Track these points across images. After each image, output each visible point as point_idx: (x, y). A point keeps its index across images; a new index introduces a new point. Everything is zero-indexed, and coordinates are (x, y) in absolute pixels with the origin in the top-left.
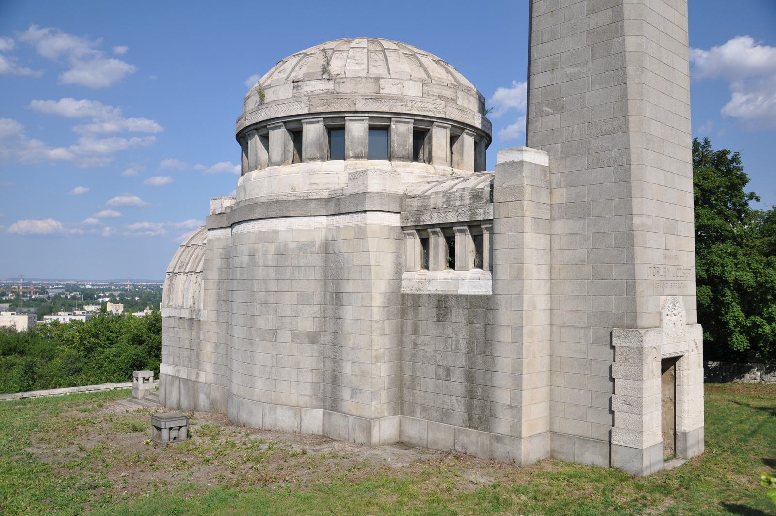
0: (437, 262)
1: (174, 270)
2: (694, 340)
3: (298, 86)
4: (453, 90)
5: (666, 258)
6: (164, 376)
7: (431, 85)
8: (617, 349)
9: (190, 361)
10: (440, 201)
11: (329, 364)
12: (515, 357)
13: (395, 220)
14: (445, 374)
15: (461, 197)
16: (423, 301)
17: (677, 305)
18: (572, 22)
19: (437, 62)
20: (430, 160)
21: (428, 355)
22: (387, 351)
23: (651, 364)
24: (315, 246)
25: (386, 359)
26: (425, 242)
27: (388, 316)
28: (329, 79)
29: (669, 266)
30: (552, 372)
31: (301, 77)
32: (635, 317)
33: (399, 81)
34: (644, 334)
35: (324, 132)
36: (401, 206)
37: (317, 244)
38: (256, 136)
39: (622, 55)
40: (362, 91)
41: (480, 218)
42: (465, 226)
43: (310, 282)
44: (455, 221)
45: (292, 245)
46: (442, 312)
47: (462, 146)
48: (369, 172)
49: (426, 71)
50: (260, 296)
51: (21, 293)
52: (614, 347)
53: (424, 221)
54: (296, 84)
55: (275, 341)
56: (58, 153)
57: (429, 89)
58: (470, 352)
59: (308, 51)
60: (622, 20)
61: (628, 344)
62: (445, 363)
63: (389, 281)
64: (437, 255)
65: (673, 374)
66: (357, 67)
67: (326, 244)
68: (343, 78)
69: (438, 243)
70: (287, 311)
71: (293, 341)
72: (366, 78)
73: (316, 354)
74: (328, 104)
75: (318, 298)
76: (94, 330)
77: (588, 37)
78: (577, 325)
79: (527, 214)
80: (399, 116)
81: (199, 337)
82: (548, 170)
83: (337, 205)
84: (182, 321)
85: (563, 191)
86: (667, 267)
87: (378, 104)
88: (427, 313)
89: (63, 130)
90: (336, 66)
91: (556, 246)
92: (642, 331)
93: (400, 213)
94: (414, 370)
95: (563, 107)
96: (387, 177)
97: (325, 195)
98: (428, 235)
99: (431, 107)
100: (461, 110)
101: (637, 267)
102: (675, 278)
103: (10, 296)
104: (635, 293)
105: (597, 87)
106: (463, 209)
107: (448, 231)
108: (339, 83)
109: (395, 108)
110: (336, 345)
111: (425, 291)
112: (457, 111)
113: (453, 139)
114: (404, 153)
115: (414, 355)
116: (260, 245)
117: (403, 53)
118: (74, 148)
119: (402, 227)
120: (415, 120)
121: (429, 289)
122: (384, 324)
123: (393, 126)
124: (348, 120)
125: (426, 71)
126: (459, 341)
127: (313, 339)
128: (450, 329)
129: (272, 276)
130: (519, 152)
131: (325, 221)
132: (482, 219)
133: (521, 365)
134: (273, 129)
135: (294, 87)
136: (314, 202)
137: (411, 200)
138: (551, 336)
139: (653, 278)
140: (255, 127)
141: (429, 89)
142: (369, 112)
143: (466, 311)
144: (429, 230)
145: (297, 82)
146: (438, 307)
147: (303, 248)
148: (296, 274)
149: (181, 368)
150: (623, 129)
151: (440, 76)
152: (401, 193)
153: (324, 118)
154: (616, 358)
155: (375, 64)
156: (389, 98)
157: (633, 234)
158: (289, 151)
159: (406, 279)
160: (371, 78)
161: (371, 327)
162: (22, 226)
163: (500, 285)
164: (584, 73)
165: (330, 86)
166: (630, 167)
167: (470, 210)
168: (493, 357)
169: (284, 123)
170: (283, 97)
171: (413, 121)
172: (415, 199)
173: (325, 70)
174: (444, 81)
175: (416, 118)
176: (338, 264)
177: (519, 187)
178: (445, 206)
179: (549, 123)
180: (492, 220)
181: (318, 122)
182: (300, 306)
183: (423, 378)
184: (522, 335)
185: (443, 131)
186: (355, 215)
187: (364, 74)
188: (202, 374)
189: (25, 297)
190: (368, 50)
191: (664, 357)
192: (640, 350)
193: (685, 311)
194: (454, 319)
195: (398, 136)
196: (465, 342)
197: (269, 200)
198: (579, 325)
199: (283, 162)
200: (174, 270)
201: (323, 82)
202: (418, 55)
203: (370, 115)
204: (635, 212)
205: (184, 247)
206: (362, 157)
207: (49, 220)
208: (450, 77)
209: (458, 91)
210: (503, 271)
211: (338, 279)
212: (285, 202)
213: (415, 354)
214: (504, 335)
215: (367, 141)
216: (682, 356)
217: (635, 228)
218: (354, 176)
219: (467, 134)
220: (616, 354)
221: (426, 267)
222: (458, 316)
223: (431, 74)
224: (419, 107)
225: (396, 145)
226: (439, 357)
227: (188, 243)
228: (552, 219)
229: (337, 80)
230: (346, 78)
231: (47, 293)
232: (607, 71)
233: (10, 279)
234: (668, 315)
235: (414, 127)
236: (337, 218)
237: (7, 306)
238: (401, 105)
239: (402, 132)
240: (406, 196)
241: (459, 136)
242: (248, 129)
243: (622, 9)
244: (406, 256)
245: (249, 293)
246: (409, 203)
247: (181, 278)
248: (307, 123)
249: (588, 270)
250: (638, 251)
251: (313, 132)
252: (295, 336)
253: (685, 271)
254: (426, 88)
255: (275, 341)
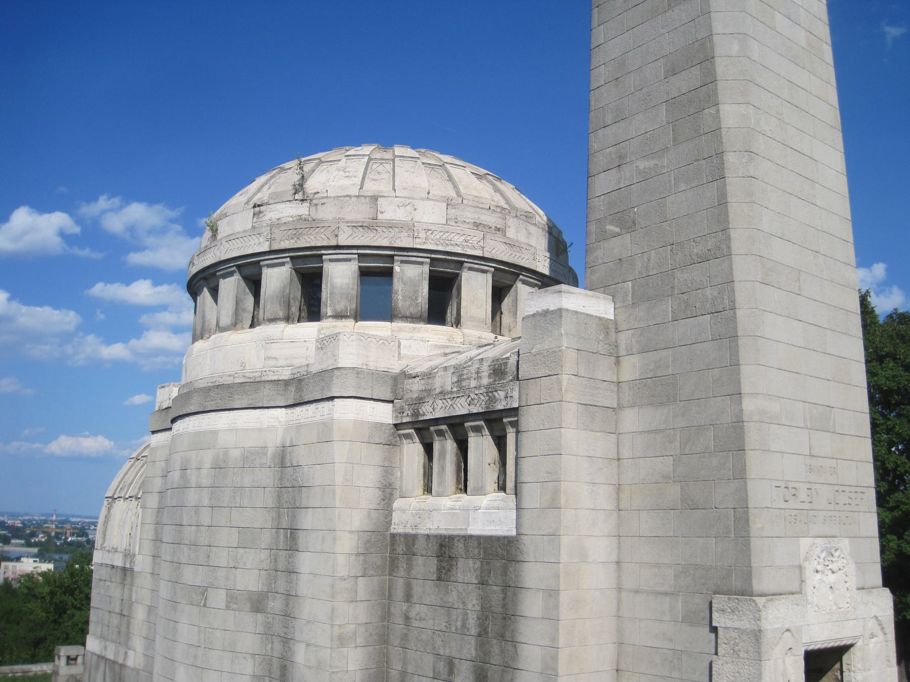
0: (441, 483)
1: (114, 493)
2: (876, 617)
3: (260, 212)
4: (500, 215)
5: (811, 470)
6: (90, 655)
7: (462, 207)
8: (720, 633)
9: (119, 632)
10: (446, 381)
11: (278, 645)
12: (548, 644)
13: (384, 414)
14: (446, 669)
15: (478, 373)
16: (420, 545)
17: (836, 554)
18: (644, 91)
19: (479, 177)
20: (457, 323)
21: (424, 637)
22: (361, 629)
23: (780, 661)
24: (265, 454)
25: (358, 641)
26: (428, 449)
27: (365, 569)
28: (303, 200)
29: (818, 486)
30: (620, 673)
31: (266, 199)
32: (748, 575)
33: (408, 201)
34: (764, 606)
35: (291, 280)
36: (394, 391)
37: (270, 451)
38: (205, 289)
39: (716, 132)
40: (349, 217)
41: (500, 406)
42: (479, 420)
43: (256, 513)
44: (464, 412)
45: (235, 454)
46: (445, 564)
47: (516, 300)
48: (341, 337)
49: (455, 187)
50: (189, 533)
51: (53, 534)
52: (714, 630)
53: (424, 414)
54: (257, 209)
55: (205, 606)
56: (117, 351)
57: (458, 213)
58: (483, 633)
59: (287, 165)
60: (714, 81)
61: (737, 624)
62: (447, 652)
63: (369, 514)
64: (443, 468)
65: (839, 677)
66: (346, 182)
67: (283, 451)
68: (323, 198)
69: (446, 447)
70: (222, 558)
71: (228, 608)
72: (358, 197)
73: (260, 629)
74: (298, 236)
75: (266, 538)
76: (67, 582)
77: (667, 111)
78: (658, 589)
79: (569, 396)
80: (405, 253)
81: (131, 596)
82: (612, 326)
83: (303, 390)
84: (114, 570)
85: (635, 359)
86: (813, 486)
87: (372, 235)
88: (425, 565)
89: (126, 322)
90: (313, 184)
91: (626, 453)
92: (760, 601)
93: (392, 402)
94: (405, 663)
95: (634, 223)
96: (372, 345)
97: (286, 375)
98: (432, 438)
99: (459, 239)
100: (511, 245)
101: (751, 486)
102: (831, 507)
103: (41, 538)
104: (748, 532)
105: (683, 187)
106: (477, 392)
107: (457, 427)
108: (316, 205)
109: (398, 241)
110: (288, 615)
111: (422, 530)
112: (503, 247)
113: (499, 293)
114: (413, 310)
115: (405, 637)
116: (193, 454)
117: (423, 163)
118: (134, 342)
119: (395, 425)
120: (432, 259)
121: (430, 526)
122: (356, 582)
123: (397, 269)
124: (326, 260)
125: (455, 187)
126: (466, 614)
127: (257, 603)
128: (455, 594)
129: (206, 502)
130: (556, 295)
131: (283, 415)
132: (502, 408)
133: (555, 658)
134: (225, 276)
135: (254, 214)
136: (268, 386)
137: (410, 381)
138: (618, 609)
139: (784, 505)
140: (201, 276)
141: (458, 213)
142: (358, 247)
143: (478, 564)
144: (432, 428)
145: (259, 206)
146: (440, 556)
147: (249, 459)
148: (238, 499)
149: (108, 643)
150: (721, 251)
151: (476, 194)
152: (396, 369)
153: (292, 258)
154: (719, 649)
155: (377, 177)
156: (391, 226)
157: (742, 428)
158: (244, 310)
159: (399, 509)
160: (365, 197)
161: (333, 587)
162: (63, 445)
163: (526, 516)
164: (663, 166)
165: (303, 210)
166: (735, 313)
167: (487, 393)
168: (515, 643)
169: (238, 267)
170: (240, 230)
171: (428, 260)
172: (417, 379)
173: (299, 187)
174: (484, 201)
175: (433, 256)
176: (295, 483)
177: (555, 352)
178: (455, 389)
179: (615, 251)
180: (516, 409)
181: (283, 264)
182: (241, 551)
183: (416, 677)
184: (557, 607)
185: (480, 276)
186: (321, 405)
187: (355, 191)
188: (131, 653)
189: (59, 539)
190: (370, 159)
191: (810, 648)
192: (757, 635)
193: (854, 566)
194: (460, 577)
195: (405, 284)
196: (475, 617)
197: (210, 384)
198: (662, 589)
199: (235, 325)
200: (114, 493)
201: (294, 204)
202: (448, 166)
203: (360, 251)
204: (746, 388)
205: (133, 461)
206: (346, 317)
207: (100, 438)
208: (498, 197)
209: (508, 218)
210: (532, 496)
211: (295, 508)
212: (229, 386)
213: (406, 635)
214: (531, 605)
215: (354, 292)
216: (852, 645)
217: (745, 418)
218: (325, 343)
219: (524, 282)
220: (719, 641)
221: (428, 489)
222: (466, 571)
223: (463, 191)
224: (438, 240)
225: (400, 297)
226: (439, 642)
227: (138, 455)
228: (620, 407)
229: (314, 202)
230: (327, 197)
231: (87, 535)
232: (696, 161)
233: (43, 515)
234: (817, 571)
235: (430, 271)
236: (298, 410)
237: (35, 550)
238: (409, 236)
239: (411, 281)
240: (406, 375)
241: (511, 286)
242: (196, 280)
243: (713, 64)
244: (402, 473)
245: (177, 528)
246: (408, 387)
247: (120, 505)
248: (269, 266)
249: (674, 492)
250: (753, 460)
251: (277, 278)
252: (232, 598)
253: (853, 495)
254: (453, 211)
255: (205, 606)
